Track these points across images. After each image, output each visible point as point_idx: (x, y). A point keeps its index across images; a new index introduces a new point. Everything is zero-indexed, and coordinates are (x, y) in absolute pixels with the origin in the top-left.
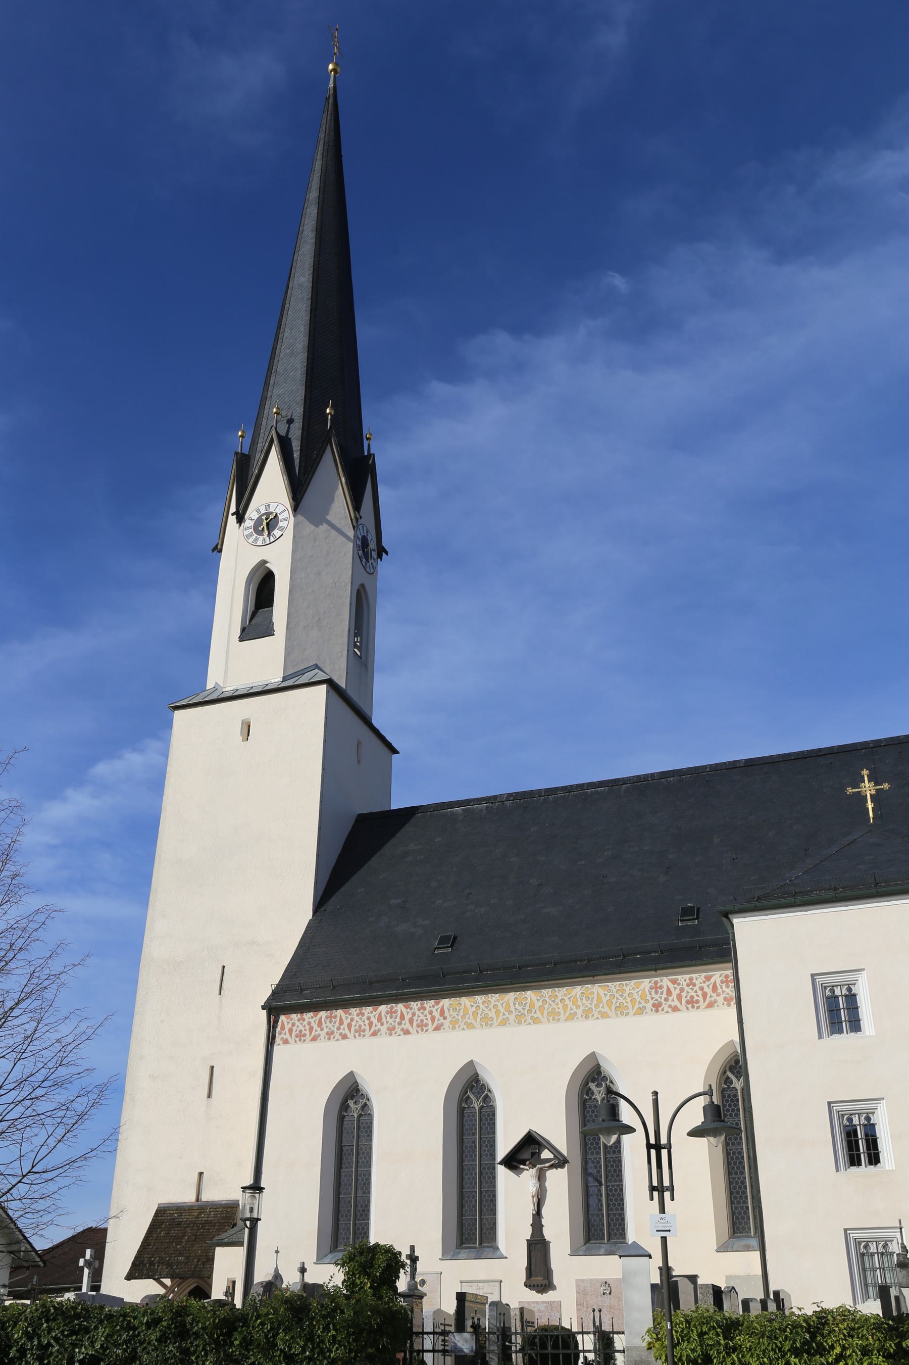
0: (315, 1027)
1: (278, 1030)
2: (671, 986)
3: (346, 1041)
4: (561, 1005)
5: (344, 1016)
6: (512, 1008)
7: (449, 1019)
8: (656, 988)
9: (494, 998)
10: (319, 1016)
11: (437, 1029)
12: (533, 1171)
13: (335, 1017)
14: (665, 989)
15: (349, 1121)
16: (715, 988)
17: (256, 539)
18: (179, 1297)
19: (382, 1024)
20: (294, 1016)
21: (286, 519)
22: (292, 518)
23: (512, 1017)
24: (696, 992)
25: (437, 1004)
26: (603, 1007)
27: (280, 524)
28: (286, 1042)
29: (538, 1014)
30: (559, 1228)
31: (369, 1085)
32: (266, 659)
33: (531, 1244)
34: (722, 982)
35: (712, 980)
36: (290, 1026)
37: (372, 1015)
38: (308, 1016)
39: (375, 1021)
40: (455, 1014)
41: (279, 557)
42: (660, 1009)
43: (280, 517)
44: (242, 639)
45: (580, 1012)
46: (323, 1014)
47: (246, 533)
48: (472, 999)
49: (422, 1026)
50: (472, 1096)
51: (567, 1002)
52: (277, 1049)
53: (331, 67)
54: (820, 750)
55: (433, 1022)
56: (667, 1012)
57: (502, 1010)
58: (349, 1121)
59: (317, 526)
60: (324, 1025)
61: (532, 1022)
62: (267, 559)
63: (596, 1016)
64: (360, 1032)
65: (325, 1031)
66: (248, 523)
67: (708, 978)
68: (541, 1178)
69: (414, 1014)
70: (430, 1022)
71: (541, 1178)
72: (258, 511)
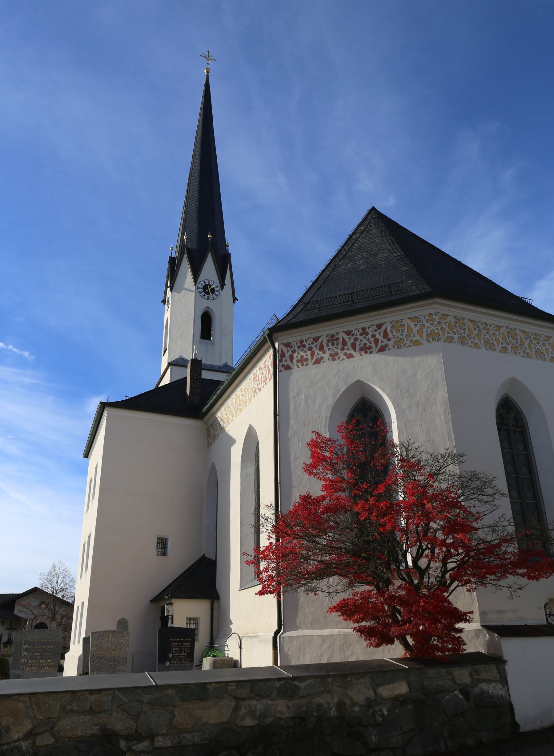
2: (346, 337)
8: (333, 340)
14: (341, 340)
16: (385, 335)
18: (422, 656)
19: (389, 340)
24: (368, 339)
26: (414, 336)
31: (254, 426)
34: (328, 341)
35: (383, 328)
39: (380, 338)
42: (336, 357)
45: (456, 337)
56: (343, 360)
59: (180, 293)
61: (411, 345)
63: (407, 345)
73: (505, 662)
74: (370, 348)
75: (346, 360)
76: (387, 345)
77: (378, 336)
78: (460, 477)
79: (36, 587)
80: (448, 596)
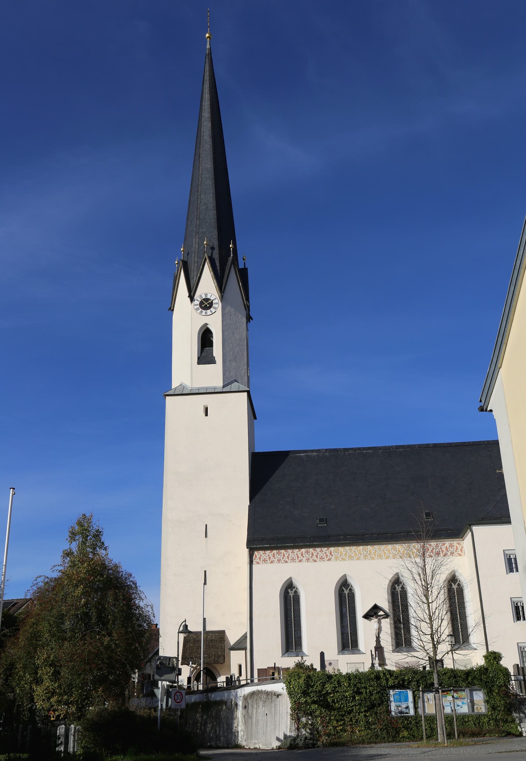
0: (272, 557)
1: (254, 557)
2: (458, 546)
4: (383, 552)
5: (400, 548)
6: (362, 553)
7: (334, 556)
9: (354, 548)
10: (330, 550)
11: (329, 560)
12: (376, 620)
13: (281, 553)
14: (455, 547)
17: (201, 312)
20: (261, 552)
21: (217, 303)
22: (220, 304)
23: (362, 557)
25: (328, 549)
27: (214, 305)
28: (258, 563)
29: (373, 556)
30: (387, 642)
32: (213, 375)
33: (376, 648)
35: (446, 545)
36: (374, 551)
37: (298, 553)
38: (268, 552)
39: (300, 556)
40: (336, 554)
41: (215, 321)
43: (214, 302)
44: (199, 363)
45: (391, 555)
47: (196, 307)
48: (344, 548)
49: (322, 558)
50: (344, 588)
51: (385, 551)
52: (254, 566)
53: (207, 35)
54: (465, 443)
55: (327, 557)
57: (358, 553)
60: (276, 556)
62: (208, 323)
64: (293, 560)
65: (277, 559)
67: (444, 544)
68: (379, 622)
69: (318, 553)
70: (325, 557)
71: (379, 622)
73: (484, 656)
74: (295, 559)
75: (314, 563)
76: (331, 558)
77: (299, 555)
79: (188, 678)
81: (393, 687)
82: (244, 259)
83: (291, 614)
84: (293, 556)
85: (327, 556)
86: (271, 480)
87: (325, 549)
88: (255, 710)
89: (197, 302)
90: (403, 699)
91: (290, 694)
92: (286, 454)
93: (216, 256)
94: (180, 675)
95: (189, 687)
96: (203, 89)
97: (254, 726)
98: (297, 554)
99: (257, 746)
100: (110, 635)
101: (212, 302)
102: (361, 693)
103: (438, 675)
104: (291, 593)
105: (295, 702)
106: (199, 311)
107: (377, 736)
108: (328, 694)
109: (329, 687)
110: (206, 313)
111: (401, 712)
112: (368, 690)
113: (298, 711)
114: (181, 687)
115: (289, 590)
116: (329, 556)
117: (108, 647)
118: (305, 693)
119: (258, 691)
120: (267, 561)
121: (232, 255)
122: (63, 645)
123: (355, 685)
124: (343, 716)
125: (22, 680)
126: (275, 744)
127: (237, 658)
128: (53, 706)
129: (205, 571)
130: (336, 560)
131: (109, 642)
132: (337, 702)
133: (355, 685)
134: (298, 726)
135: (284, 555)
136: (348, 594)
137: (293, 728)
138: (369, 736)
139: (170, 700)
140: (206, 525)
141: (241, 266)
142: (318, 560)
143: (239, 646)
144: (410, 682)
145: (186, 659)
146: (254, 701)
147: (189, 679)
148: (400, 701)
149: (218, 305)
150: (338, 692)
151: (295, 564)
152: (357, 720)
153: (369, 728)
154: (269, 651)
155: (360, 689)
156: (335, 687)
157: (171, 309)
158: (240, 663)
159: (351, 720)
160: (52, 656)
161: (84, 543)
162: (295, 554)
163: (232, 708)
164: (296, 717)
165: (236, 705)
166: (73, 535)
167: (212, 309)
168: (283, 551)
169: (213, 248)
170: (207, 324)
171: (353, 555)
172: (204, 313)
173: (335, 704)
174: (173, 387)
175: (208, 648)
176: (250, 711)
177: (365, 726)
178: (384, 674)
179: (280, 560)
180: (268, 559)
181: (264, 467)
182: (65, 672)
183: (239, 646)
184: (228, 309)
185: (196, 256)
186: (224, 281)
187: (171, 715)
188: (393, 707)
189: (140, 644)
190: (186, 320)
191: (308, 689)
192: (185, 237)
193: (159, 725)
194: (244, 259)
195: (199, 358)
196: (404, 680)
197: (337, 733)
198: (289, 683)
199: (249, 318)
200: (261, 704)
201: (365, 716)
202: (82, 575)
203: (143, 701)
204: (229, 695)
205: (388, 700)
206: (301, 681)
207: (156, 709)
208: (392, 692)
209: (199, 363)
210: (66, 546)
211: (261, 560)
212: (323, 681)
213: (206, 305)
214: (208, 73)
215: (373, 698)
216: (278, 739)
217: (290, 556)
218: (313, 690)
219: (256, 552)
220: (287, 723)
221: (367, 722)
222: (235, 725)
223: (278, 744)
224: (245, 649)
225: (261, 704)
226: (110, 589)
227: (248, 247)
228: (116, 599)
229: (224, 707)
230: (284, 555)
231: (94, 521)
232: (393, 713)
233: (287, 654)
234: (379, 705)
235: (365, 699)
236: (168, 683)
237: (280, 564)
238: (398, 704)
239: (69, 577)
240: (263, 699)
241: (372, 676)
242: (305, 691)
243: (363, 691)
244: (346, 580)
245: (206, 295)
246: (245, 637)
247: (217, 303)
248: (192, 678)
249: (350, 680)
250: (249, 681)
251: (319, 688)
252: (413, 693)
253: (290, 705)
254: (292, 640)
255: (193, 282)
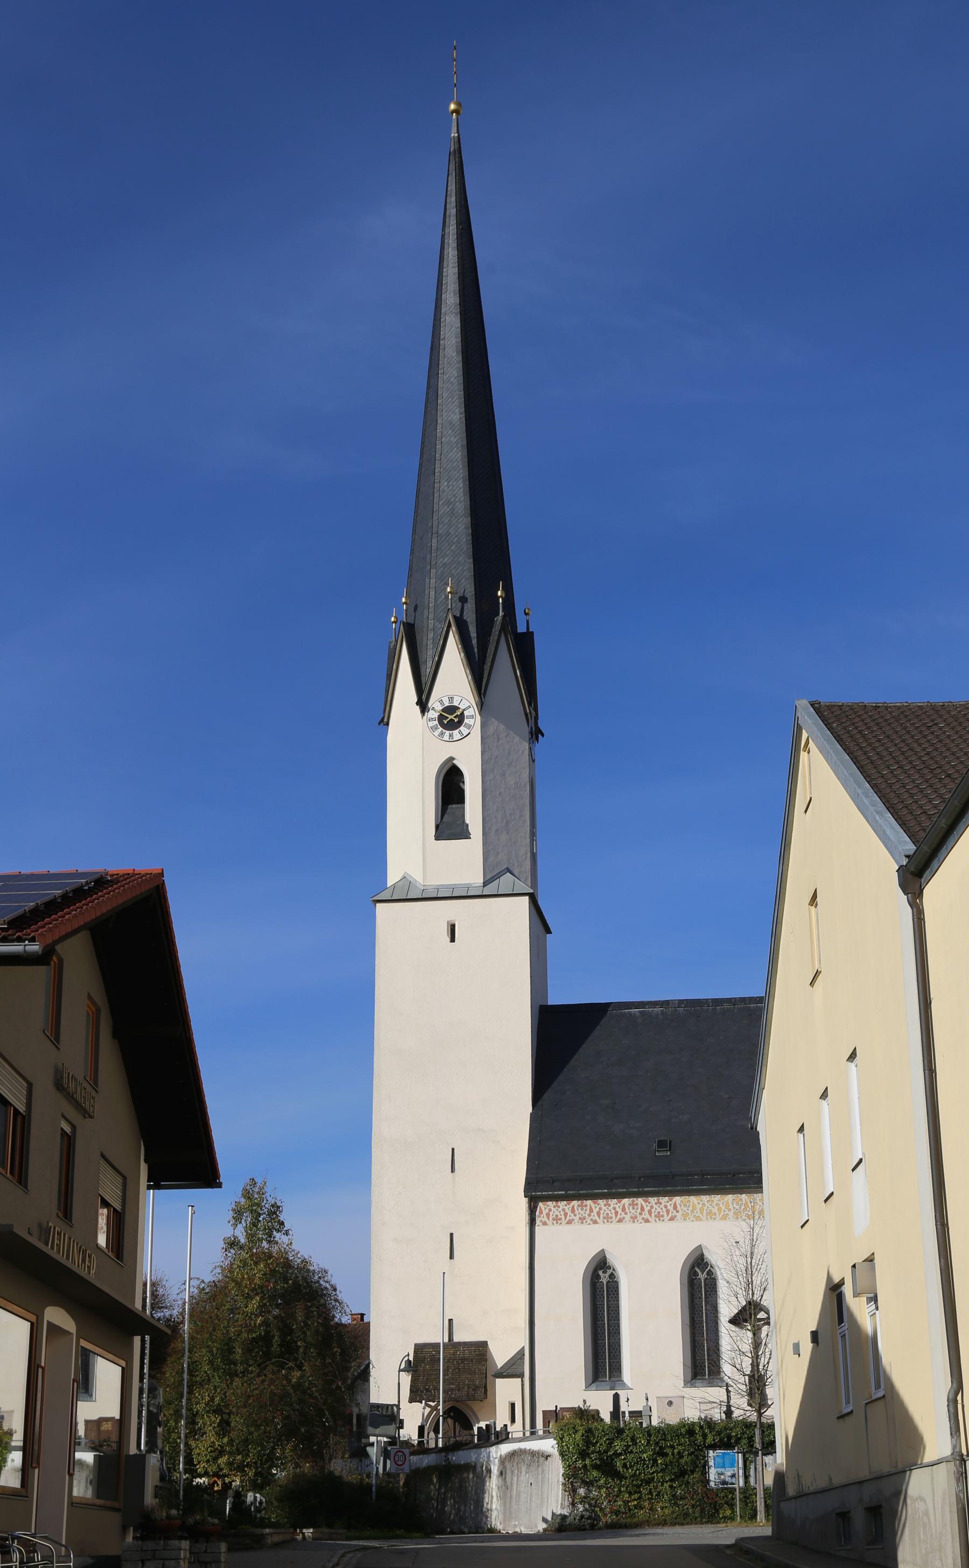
0: (569, 1213)
1: (537, 1213)
3: (596, 1225)
5: (593, 1206)
6: (731, 1207)
7: (681, 1213)
9: (716, 1198)
11: (672, 1219)
13: (586, 1206)
15: (601, 1289)
17: (442, 734)
20: (550, 1203)
21: (472, 717)
22: (478, 717)
27: (466, 721)
28: (545, 1224)
31: (614, 1259)
32: (464, 860)
38: (562, 1204)
39: (620, 1211)
40: (685, 1209)
41: (468, 752)
43: (466, 713)
44: (438, 838)
46: (575, 1203)
47: (431, 724)
48: (698, 1197)
49: (659, 1216)
52: (538, 1229)
57: (723, 1208)
58: (601, 1289)
60: (576, 1212)
62: (454, 756)
64: (607, 1218)
65: (578, 1216)
66: (433, 714)
69: (652, 1207)
70: (665, 1214)
72: (441, 702)
75: (644, 1224)
76: (675, 1216)
77: (617, 1209)
78: (6, 1443)
80: (409, 895)
81: (714, 1447)
82: (526, 614)
83: (603, 1314)
84: (608, 1211)
85: (668, 1212)
86: (573, 1062)
87: (664, 1200)
88: (515, 1479)
89: (433, 714)
90: (727, 1462)
91: (562, 1454)
92: (601, 1009)
93: (470, 616)
94: (402, 1427)
95: (421, 1443)
96: (443, 236)
97: (514, 1501)
98: (614, 1208)
99: (518, 1530)
100: (300, 1367)
101: (462, 713)
102: (666, 1455)
103: (763, 1432)
104: (604, 1278)
105: (569, 1466)
106: (437, 733)
107: (686, 1515)
108: (617, 1455)
109: (618, 1446)
110: (451, 735)
111: (724, 1483)
112: (676, 1451)
113: (573, 1478)
114: (407, 1443)
115: (601, 1273)
116: (672, 1213)
117: (298, 1386)
118: (583, 1455)
119: (521, 1450)
120: (560, 1219)
121: (501, 614)
122: (231, 1383)
123: (657, 1444)
124: (638, 1486)
125: (173, 1432)
126: (541, 1526)
127: (506, 1391)
128: (221, 1470)
129: (452, 1235)
130: (685, 1220)
131: (299, 1379)
132: (631, 1466)
133: (657, 1444)
134: (573, 1501)
135: (591, 1210)
136: (706, 1279)
137: (567, 1503)
138: (675, 1515)
139: (388, 1462)
140: (453, 1149)
141: (521, 629)
142: (652, 1219)
143: (512, 1370)
144: (740, 1439)
145: (417, 1391)
146: (515, 1464)
147: (421, 1429)
148: (724, 1467)
149: (473, 719)
150: (631, 1452)
151: (612, 1225)
152: (659, 1493)
153: (675, 1504)
154: (563, 1381)
155: (664, 1448)
156: (628, 1446)
157: (384, 722)
158: (512, 1400)
159: (650, 1493)
160: (217, 1400)
161: (255, 1225)
162: (611, 1208)
163: (481, 1475)
164: (571, 1489)
165: (489, 1471)
166: (238, 1215)
167: (462, 728)
168: (589, 1202)
169: (463, 600)
170: (452, 759)
171: (715, 1210)
172: (446, 737)
173: (628, 1469)
174: (390, 883)
175: (456, 1373)
176: (508, 1480)
177: (670, 1501)
178: (701, 1427)
179: (585, 1218)
180: (563, 1217)
181: (561, 1035)
182: (237, 1422)
183: (512, 1370)
184: (494, 724)
185: (431, 616)
186: (487, 667)
187: (390, 1482)
188: (713, 1474)
189: (344, 1381)
190: (413, 750)
191: (588, 1448)
192: (410, 568)
193: (374, 1495)
194: (526, 614)
195: (437, 827)
196: (729, 1437)
197: (630, 1510)
198: (561, 1439)
199: (536, 733)
200: (524, 1468)
201: (671, 1487)
202: (257, 1281)
203: (353, 1464)
204: (478, 1458)
205: (706, 1464)
206: (578, 1437)
207: (369, 1476)
208: (711, 1453)
209: (438, 838)
210: (228, 1232)
211: (551, 1218)
212: (611, 1436)
213: (451, 719)
214: (453, 199)
215: (683, 1461)
216: (545, 1520)
217: (602, 1212)
218: (600, 1450)
219: (540, 1204)
220: (557, 1496)
221: (674, 1496)
222: (486, 1500)
223: (545, 1526)
224: (521, 1376)
225: (524, 1468)
226: (299, 1300)
227: (534, 592)
228: (308, 1316)
229: (471, 1476)
230: (591, 1210)
231: (269, 1190)
232: (712, 1484)
233: (594, 1385)
234: (693, 1472)
235: (671, 1462)
236: (385, 1439)
237: (585, 1226)
238: (720, 1470)
239: (237, 1283)
240: (526, 1461)
241: (683, 1430)
242: (584, 1450)
243: (669, 1451)
244: (702, 1255)
245: (451, 699)
246: (521, 1353)
247: (472, 717)
248: (426, 1428)
249: (650, 1435)
250: (528, 1434)
251: (604, 1448)
252: (744, 1456)
253: (562, 1471)
254: (604, 1360)
255: (427, 670)
